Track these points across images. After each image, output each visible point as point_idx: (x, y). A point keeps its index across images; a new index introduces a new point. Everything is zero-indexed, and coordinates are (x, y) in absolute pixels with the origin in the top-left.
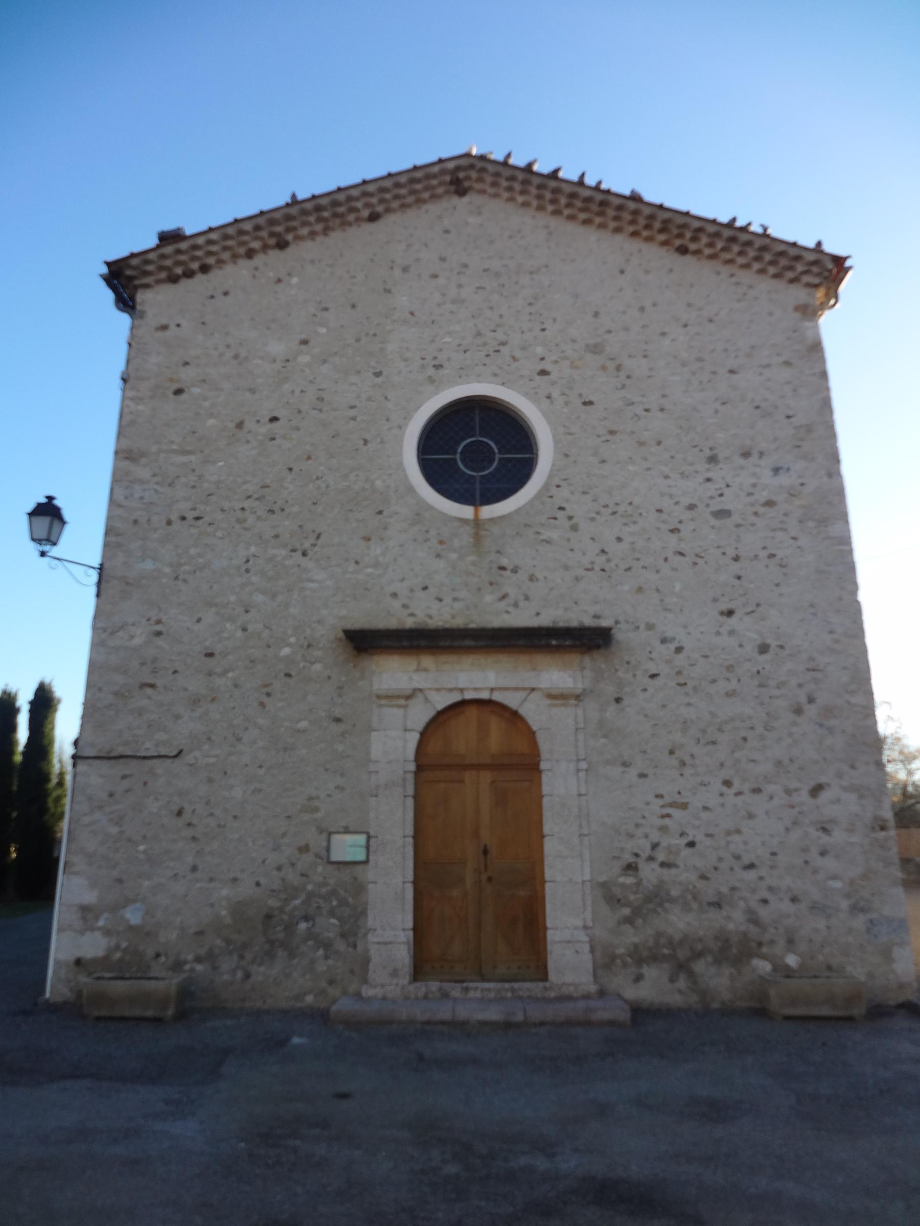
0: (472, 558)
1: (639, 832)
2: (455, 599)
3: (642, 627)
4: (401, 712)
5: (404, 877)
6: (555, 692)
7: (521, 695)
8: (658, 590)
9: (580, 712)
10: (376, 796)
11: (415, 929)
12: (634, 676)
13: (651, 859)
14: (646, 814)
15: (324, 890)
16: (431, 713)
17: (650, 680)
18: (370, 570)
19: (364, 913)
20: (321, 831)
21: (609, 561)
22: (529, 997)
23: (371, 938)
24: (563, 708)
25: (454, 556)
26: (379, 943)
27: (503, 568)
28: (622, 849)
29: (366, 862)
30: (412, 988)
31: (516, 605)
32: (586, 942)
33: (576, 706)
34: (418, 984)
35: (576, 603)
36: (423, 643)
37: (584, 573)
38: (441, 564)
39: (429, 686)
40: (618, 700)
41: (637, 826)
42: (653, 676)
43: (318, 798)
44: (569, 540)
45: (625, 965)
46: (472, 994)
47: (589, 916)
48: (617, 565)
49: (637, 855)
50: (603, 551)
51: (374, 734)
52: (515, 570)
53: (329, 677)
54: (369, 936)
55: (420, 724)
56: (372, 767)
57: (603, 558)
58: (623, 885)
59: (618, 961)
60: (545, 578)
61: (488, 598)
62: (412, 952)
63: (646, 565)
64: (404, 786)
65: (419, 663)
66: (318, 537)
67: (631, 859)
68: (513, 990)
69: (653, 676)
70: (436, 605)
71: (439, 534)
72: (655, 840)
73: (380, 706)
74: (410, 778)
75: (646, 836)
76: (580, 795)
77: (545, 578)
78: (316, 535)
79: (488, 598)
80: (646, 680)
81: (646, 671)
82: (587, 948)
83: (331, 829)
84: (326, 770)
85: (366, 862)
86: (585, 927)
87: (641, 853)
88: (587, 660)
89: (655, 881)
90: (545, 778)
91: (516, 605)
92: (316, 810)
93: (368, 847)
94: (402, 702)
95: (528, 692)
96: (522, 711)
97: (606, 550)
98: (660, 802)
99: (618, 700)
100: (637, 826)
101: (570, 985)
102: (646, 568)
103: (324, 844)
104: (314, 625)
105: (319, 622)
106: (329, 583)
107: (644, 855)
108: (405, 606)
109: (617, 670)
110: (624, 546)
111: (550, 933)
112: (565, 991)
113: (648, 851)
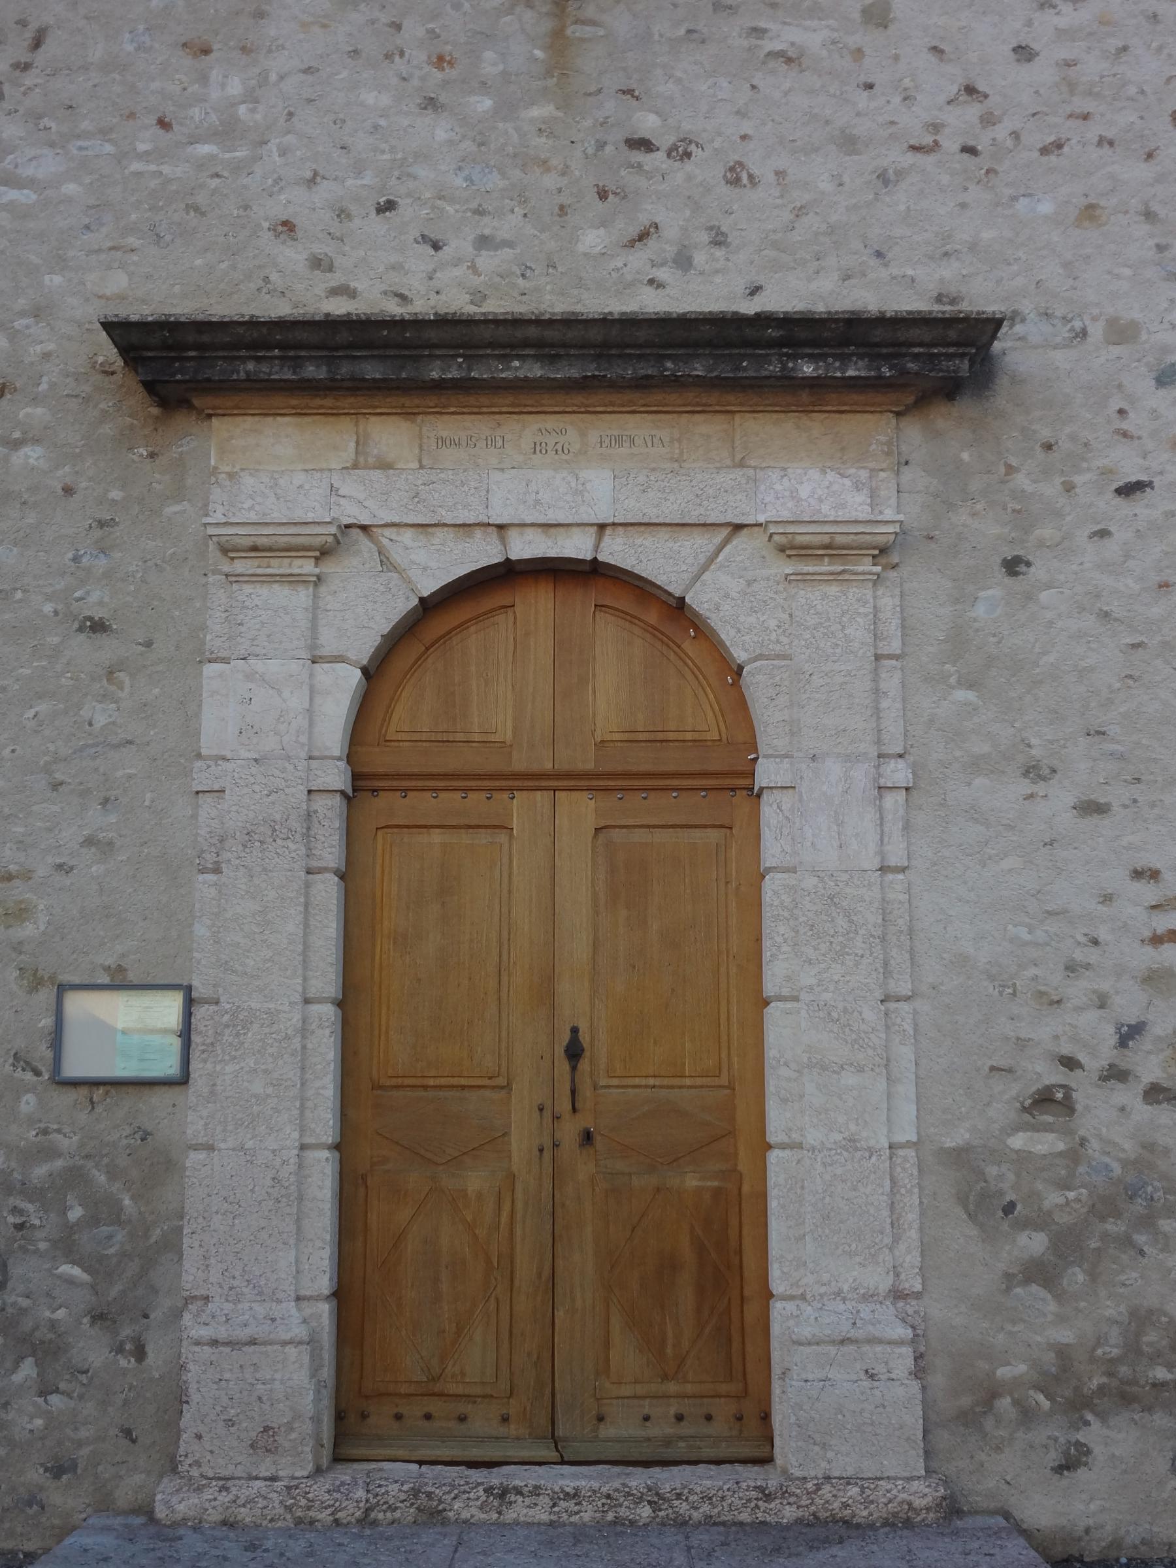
0: (541, 111)
1: (1078, 990)
2: (484, 242)
3: (1097, 331)
4: (302, 596)
5: (302, 1130)
6: (806, 534)
7: (701, 544)
8: (1149, 215)
9: (888, 602)
10: (217, 870)
11: (340, 1295)
12: (1069, 488)
13: (1116, 1074)
14: (1103, 934)
15: (40, 1171)
16: (404, 604)
17: (1119, 501)
18: (205, 149)
19: (172, 1245)
20: (36, 983)
21: (988, 120)
22: (709, 1522)
23: (193, 1327)
24: (833, 590)
25: (484, 104)
26: (214, 1343)
27: (644, 145)
28: (1022, 1044)
29: (183, 1080)
30: (319, 1489)
31: (683, 261)
32: (901, 1343)
33: (878, 580)
34: (344, 1474)
35: (879, 254)
36: (373, 371)
37: (910, 158)
38: (442, 130)
39: (386, 517)
40: (1013, 566)
41: (1071, 968)
42: (1129, 490)
43: (26, 875)
44: (859, 53)
45: (1027, 1416)
46: (519, 1510)
47: (912, 1260)
48: (1016, 135)
49: (1070, 1063)
50: (970, 90)
51: (210, 669)
52: (681, 152)
53: (68, 491)
54: (187, 1319)
55: (365, 646)
56: (203, 778)
57: (972, 111)
58: (1023, 1158)
59: (1004, 1403)
60: (780, 174)
61: (592, 240)
62: (327, 1372)
63: (1109, 134)
64: (308, 835)
65: (361, 444)
66: (37, 44)
67: (1054, 1076)
68: (656, 1500)
69: (1129, 490)
70: (420, 260)
71: (433, 35)
72: (1131, 1017)
73: (232, 578)
74: (331, 811)
75: (1102, 1003)
76: (883, 869)
77: (780, 174)
78: (29, 34)
79: (592, 240)
80: (1108, 503)
81: (1107, 472)
82: (903, 1360)
83: (66, 978)
84: (56, 786)
85: (183, 1080)
86: (898, 1295)
87: (1082, 1057)
88: (913, 434)
89: (1129, 1147)
90: (769, 811)
91: (683, 261)
92: (21, 913)
93: (186, 1033)
94: (307, 567)
95: (725, 532)
96: (700, 600)
97: (981, 86)
98: (1149, 893)
99: (1013, 566)
100: (1071, 968)
101: (848, 1481)
102: (1111, 143)
103: (47, 1022)
104: (19, 324)
105: (37, 313)
106: (71, 188)
107: (1094, 1064)
108: (318, 263)
109: (1010, 469)
110: (1042, 72)
111: (779, 1310)
112: (830, 1500)
113: (1106, 1051)
